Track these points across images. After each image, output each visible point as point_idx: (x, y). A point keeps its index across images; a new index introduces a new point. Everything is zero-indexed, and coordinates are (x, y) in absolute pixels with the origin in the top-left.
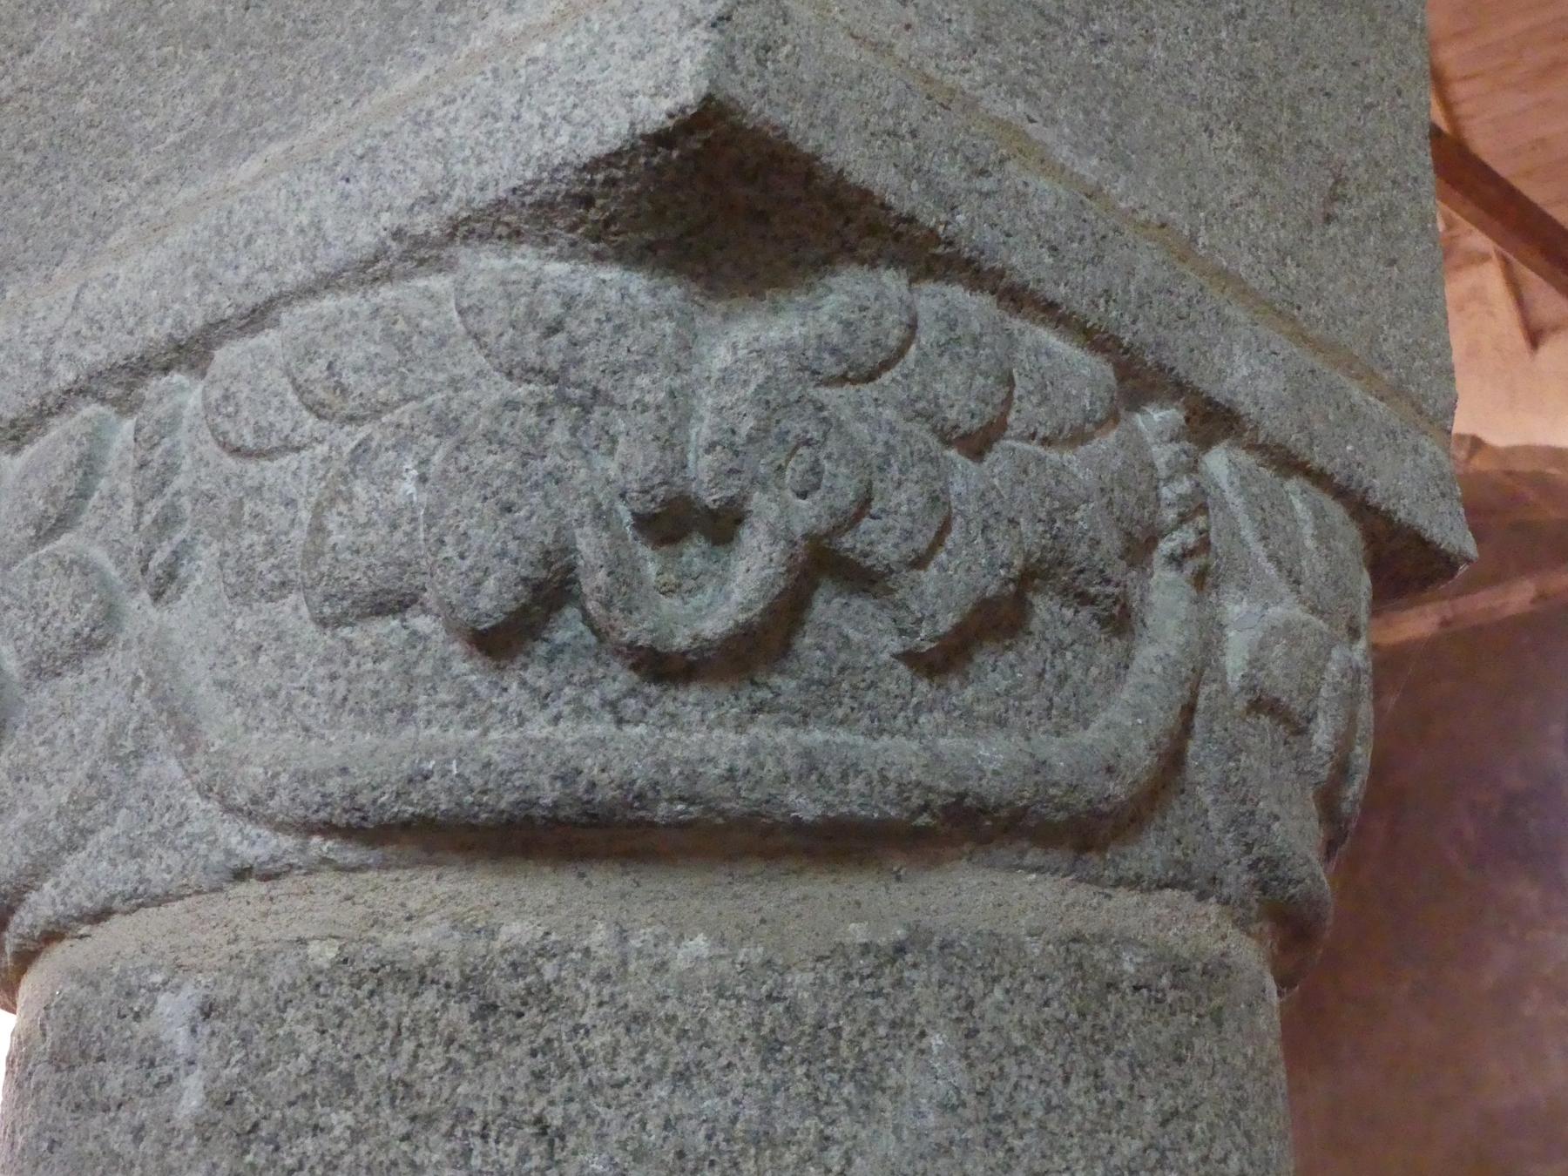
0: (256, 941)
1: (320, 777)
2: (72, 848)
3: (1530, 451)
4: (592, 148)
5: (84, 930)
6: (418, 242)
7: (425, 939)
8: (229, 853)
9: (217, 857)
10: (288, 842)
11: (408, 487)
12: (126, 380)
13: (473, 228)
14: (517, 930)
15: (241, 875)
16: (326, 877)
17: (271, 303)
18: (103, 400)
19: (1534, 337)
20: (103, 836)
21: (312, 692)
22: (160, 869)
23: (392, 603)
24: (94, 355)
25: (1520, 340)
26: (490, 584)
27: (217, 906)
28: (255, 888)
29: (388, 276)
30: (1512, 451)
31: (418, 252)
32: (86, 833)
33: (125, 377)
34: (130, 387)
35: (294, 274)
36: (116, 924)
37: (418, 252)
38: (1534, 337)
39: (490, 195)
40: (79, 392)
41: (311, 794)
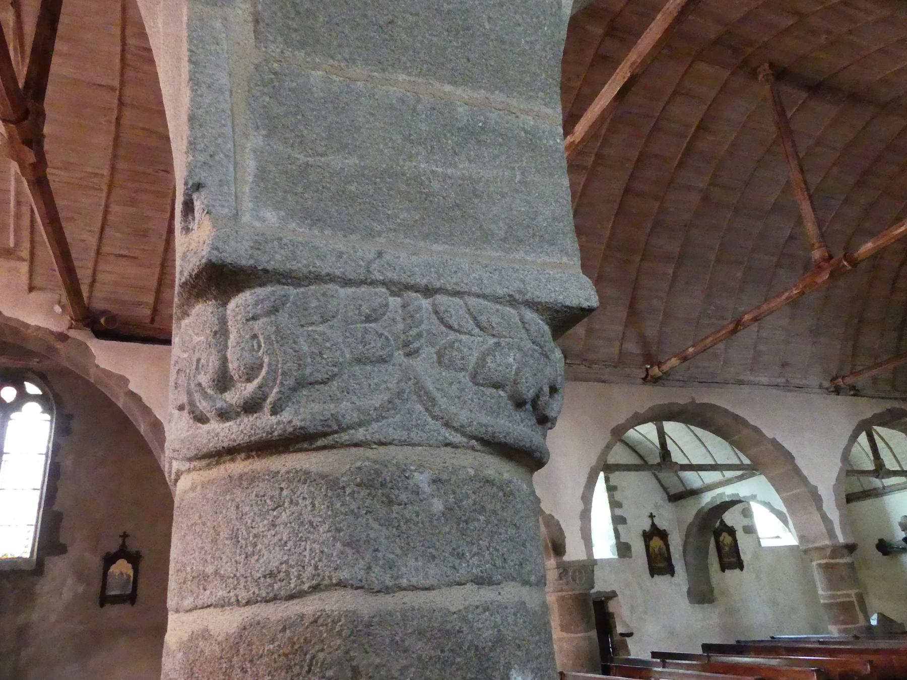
0: (453, 464)
1: (486, 426)
2: (377, 420)
3: (18, 321)
4: (568, 303)
5: (375, 446)
6: (515, 300)
7: (491, 473)
8: (446, 438)
9: (441, 438)
10: (465, 440)
11: (511, 360)
12: (398, 288)
13: (533, 305)
14: (506, 476)
15: (447, 445)
16: (469, 452)
17: (464, 293)
18: (388, 289)
19: (31, 289)
20: (390, 420)
21: (472, 401)
22: (415, 436)
23: (497, 386)
24: (391, 275)
25: (26, 288)
26: (531, 391)
27: (436, 452)
28: (449, 449)
29: (500, 303)
30: (10, 319)
31: (512, 301)
32: (384, 418)
33: (402, 287)
34: (400, 290)
35: (475, 289)
36: (392, 448)
37: (512, 301)
38: (31, 289)
39: (539, 300)
40: (384, 283)
41: (483, 430)
